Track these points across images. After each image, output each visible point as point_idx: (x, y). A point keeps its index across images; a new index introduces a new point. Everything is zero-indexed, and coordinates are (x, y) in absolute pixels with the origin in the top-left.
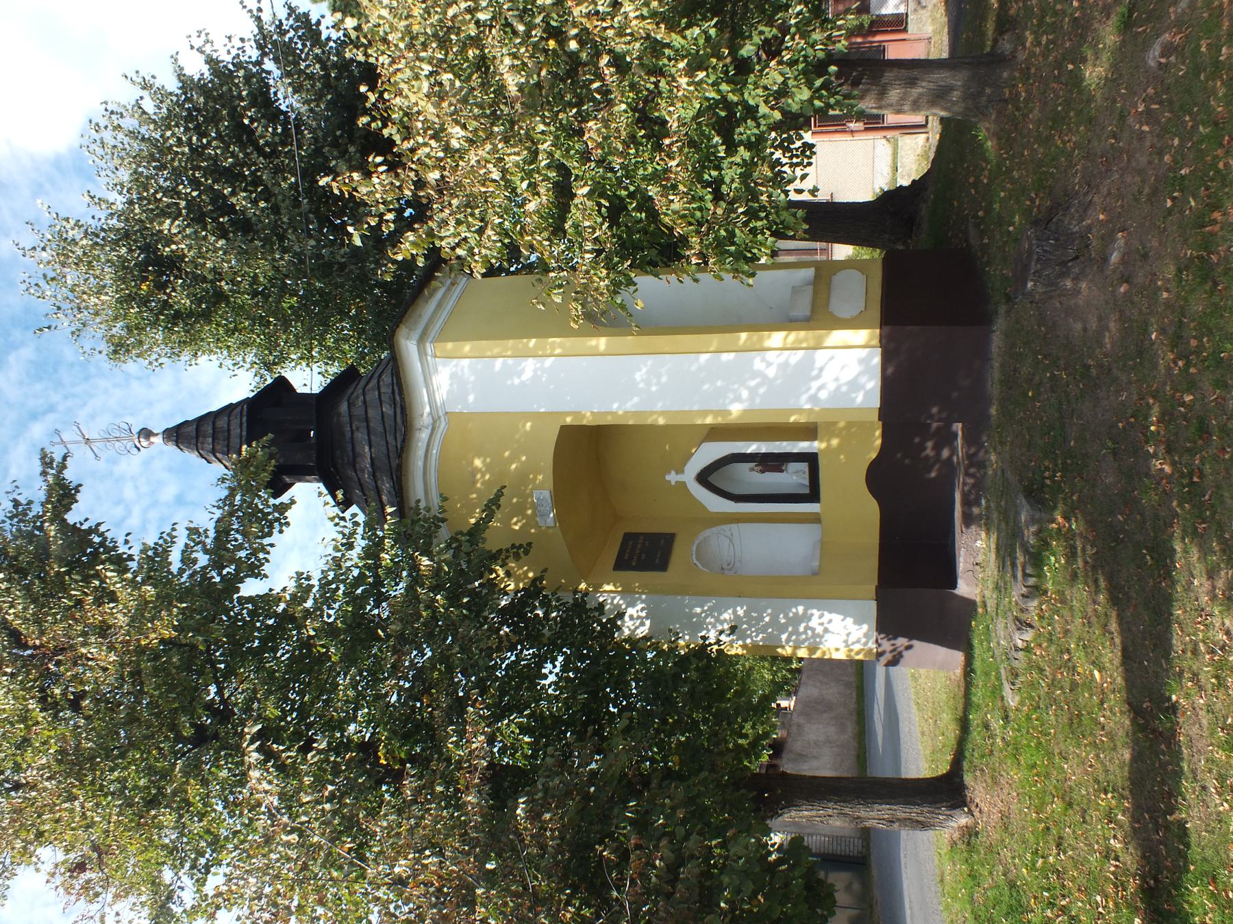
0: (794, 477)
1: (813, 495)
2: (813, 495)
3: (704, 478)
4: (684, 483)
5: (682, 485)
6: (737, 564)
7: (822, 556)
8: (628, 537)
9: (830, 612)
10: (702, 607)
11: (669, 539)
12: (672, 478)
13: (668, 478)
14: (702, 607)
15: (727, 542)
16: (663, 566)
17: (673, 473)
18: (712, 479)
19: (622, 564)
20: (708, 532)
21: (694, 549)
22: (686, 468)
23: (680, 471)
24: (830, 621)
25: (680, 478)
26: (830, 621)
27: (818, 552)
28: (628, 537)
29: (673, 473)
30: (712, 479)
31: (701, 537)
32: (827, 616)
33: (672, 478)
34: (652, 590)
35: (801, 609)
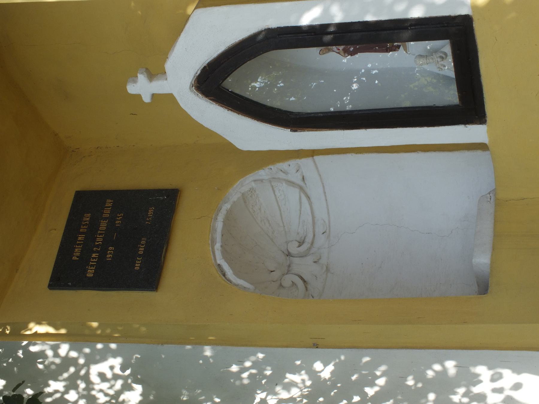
0: (425, 70)
1: (469, 107)
2: (469, 107)
3: (213, 81)
4: (170, 98)
5: (166, 101)
6: (321, 241)
7: (498, 236)
8: (86, 202)
9: (518, 371)
10: (240, 362)
11: (166, 202)
12: (142, 87)
13: (132, 89)
14: (240, 362)
15: (293, 194)
16: (148, 277)
17: (142, 78)
18: (231, 83)
19: (66, 276)
20: (247, 183)
21: (219, 225)
22: (168, 66)
23: (156, 72)
24: (517, 386)
25: (159, 87)
26: (517, 386)
27: (487, 228)
28: (86, 202)
29: (142, 78)
30: (231, 83)
31: (235, 194)
32: (509, 378)
33: (142, 87)
34: (124, 336)
35: (450, 365)
